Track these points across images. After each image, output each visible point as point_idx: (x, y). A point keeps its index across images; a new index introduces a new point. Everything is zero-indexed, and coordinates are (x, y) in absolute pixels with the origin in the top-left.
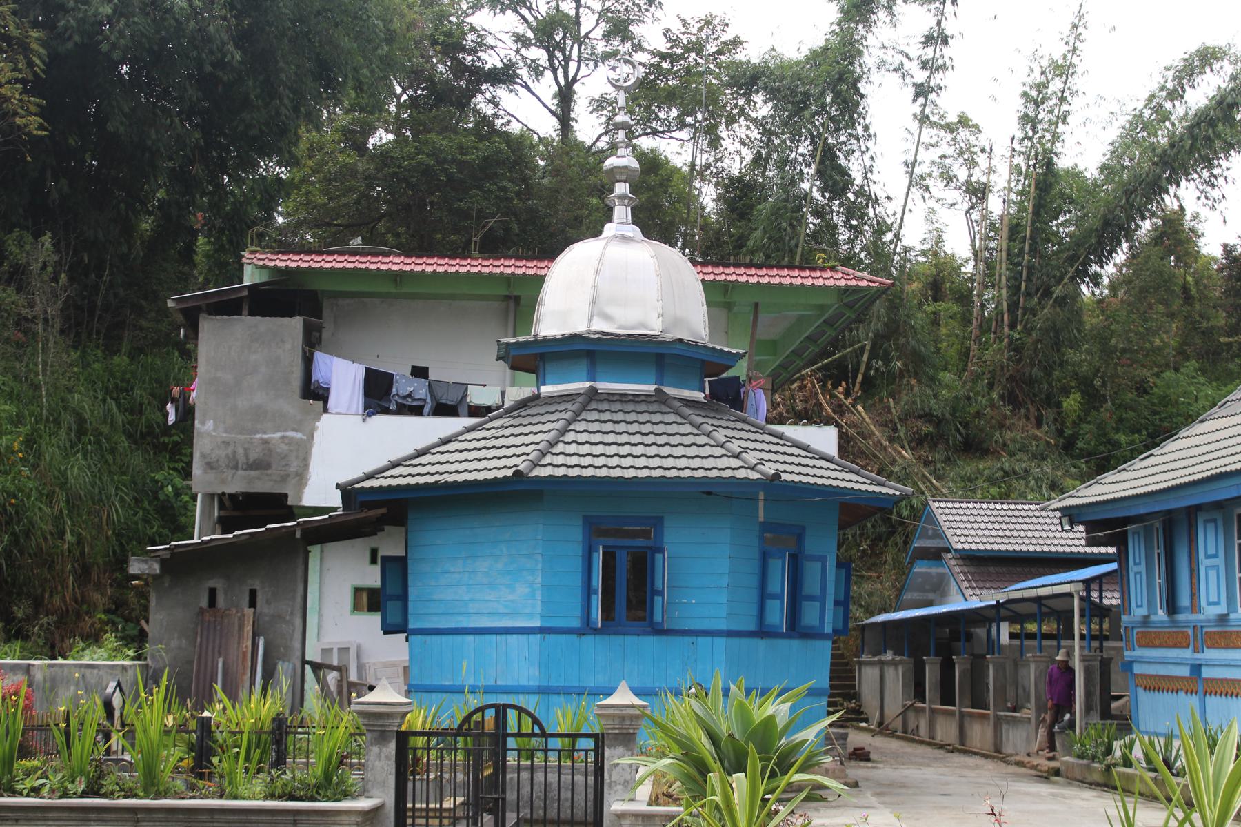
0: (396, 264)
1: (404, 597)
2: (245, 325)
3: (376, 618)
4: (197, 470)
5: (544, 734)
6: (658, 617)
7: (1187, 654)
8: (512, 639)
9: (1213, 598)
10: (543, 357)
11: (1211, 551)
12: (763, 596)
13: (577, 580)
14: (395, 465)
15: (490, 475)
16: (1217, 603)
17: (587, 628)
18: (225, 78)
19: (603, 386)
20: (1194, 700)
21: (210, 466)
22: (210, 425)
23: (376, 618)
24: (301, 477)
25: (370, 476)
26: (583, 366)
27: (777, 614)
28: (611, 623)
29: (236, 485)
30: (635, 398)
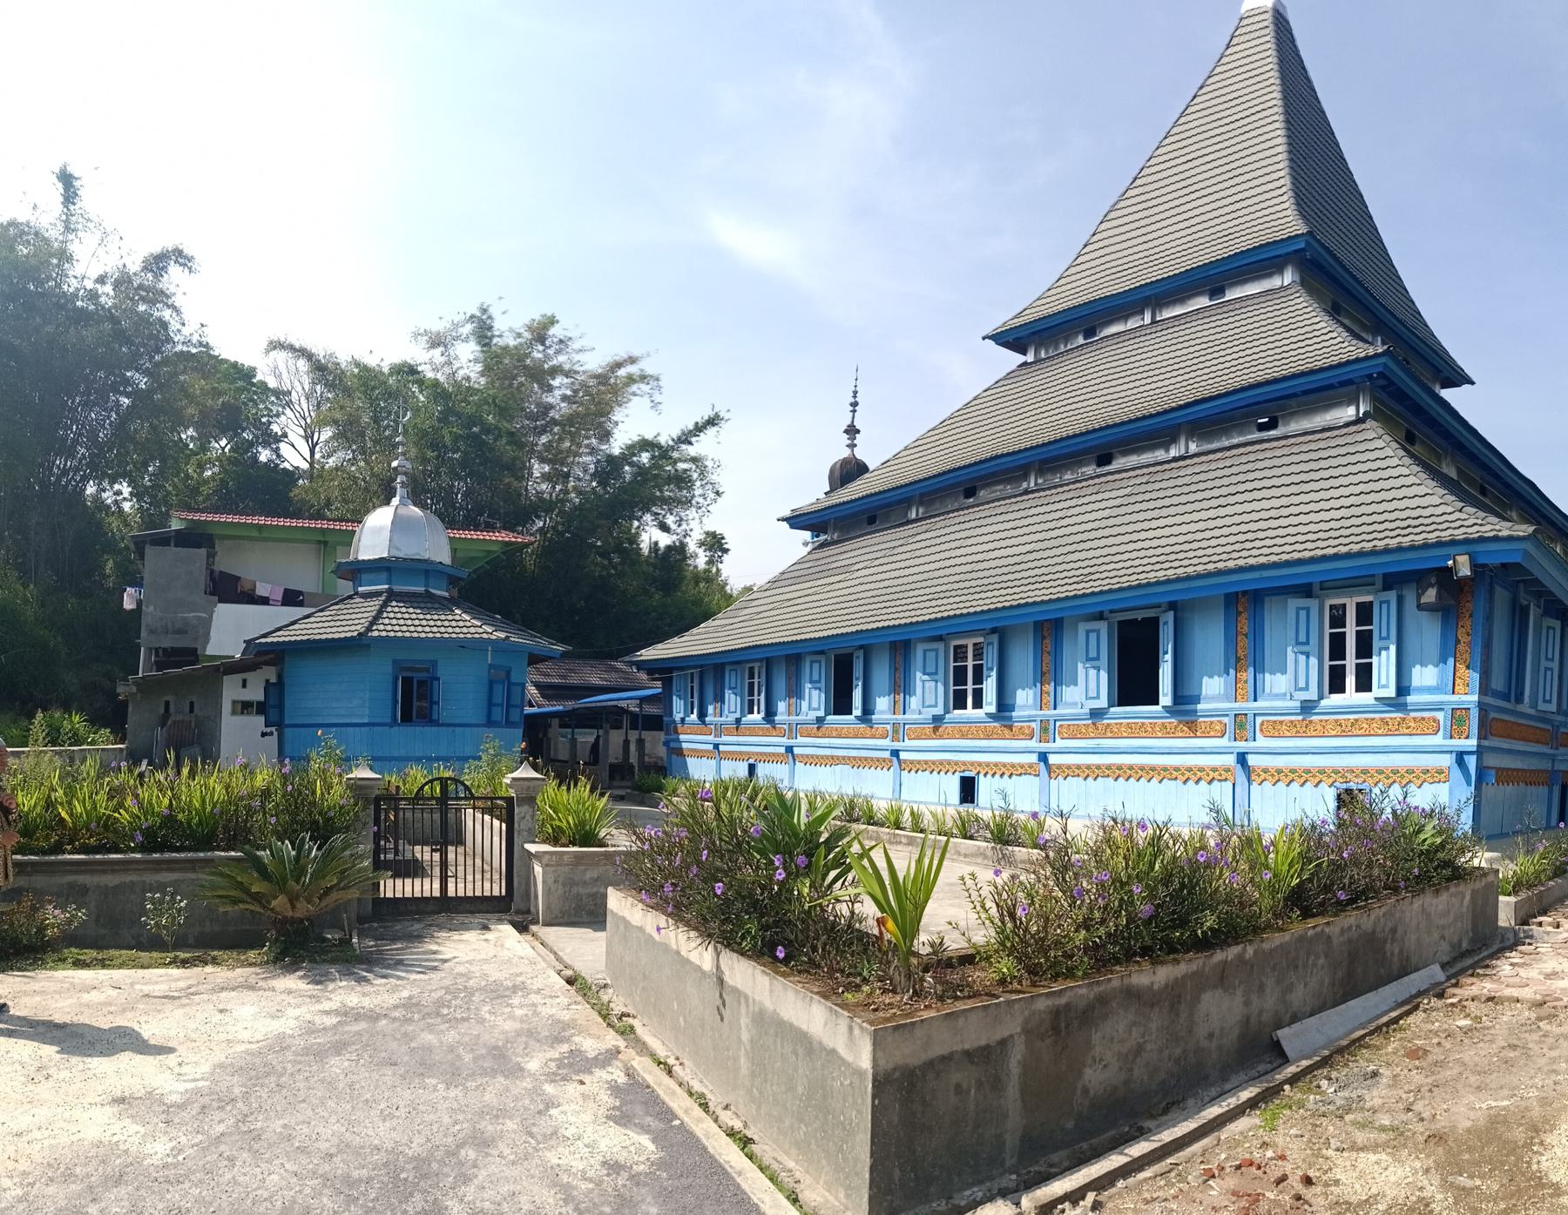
0: (261, 520)
1: (281, 706)
2: (172, 551)
3: (262, 718)
4: (144, 634)
5: (473, 797)
6: (435, 717)
7: (711, 738)
8: (351, 730)
9: (1383, 682)
10: (359, 571)
11: (815, 677)
12: (490, 704)
13: (389, 695)
14: (279, 629)
15: (342, 635)
16: (1307, 688)
17: (394, 722)
18: (126, 490)
19: (397, 588)
20: (713, 762)
21: (151, 632)
22: (151, 608)
23: (262, 718)
24: (206, 638)
25: (264, 636)
26: (384, 576)
27: (498, 714)
28: (407, 718)
29: (167, 643)
30: (414, 595)
